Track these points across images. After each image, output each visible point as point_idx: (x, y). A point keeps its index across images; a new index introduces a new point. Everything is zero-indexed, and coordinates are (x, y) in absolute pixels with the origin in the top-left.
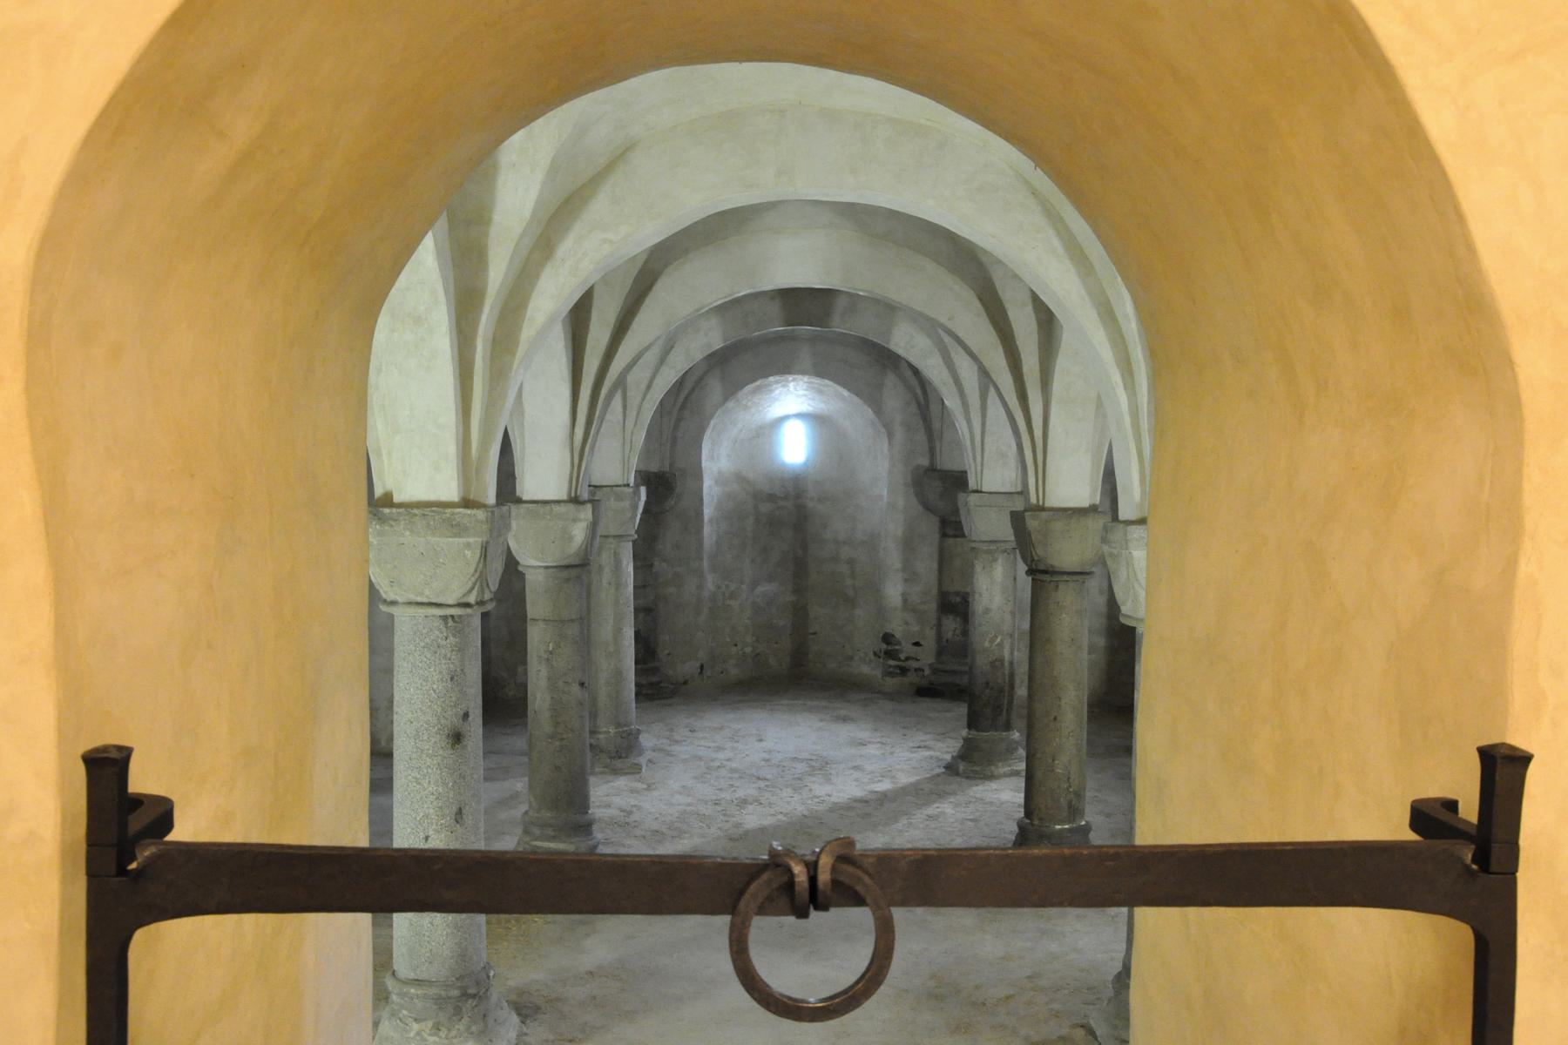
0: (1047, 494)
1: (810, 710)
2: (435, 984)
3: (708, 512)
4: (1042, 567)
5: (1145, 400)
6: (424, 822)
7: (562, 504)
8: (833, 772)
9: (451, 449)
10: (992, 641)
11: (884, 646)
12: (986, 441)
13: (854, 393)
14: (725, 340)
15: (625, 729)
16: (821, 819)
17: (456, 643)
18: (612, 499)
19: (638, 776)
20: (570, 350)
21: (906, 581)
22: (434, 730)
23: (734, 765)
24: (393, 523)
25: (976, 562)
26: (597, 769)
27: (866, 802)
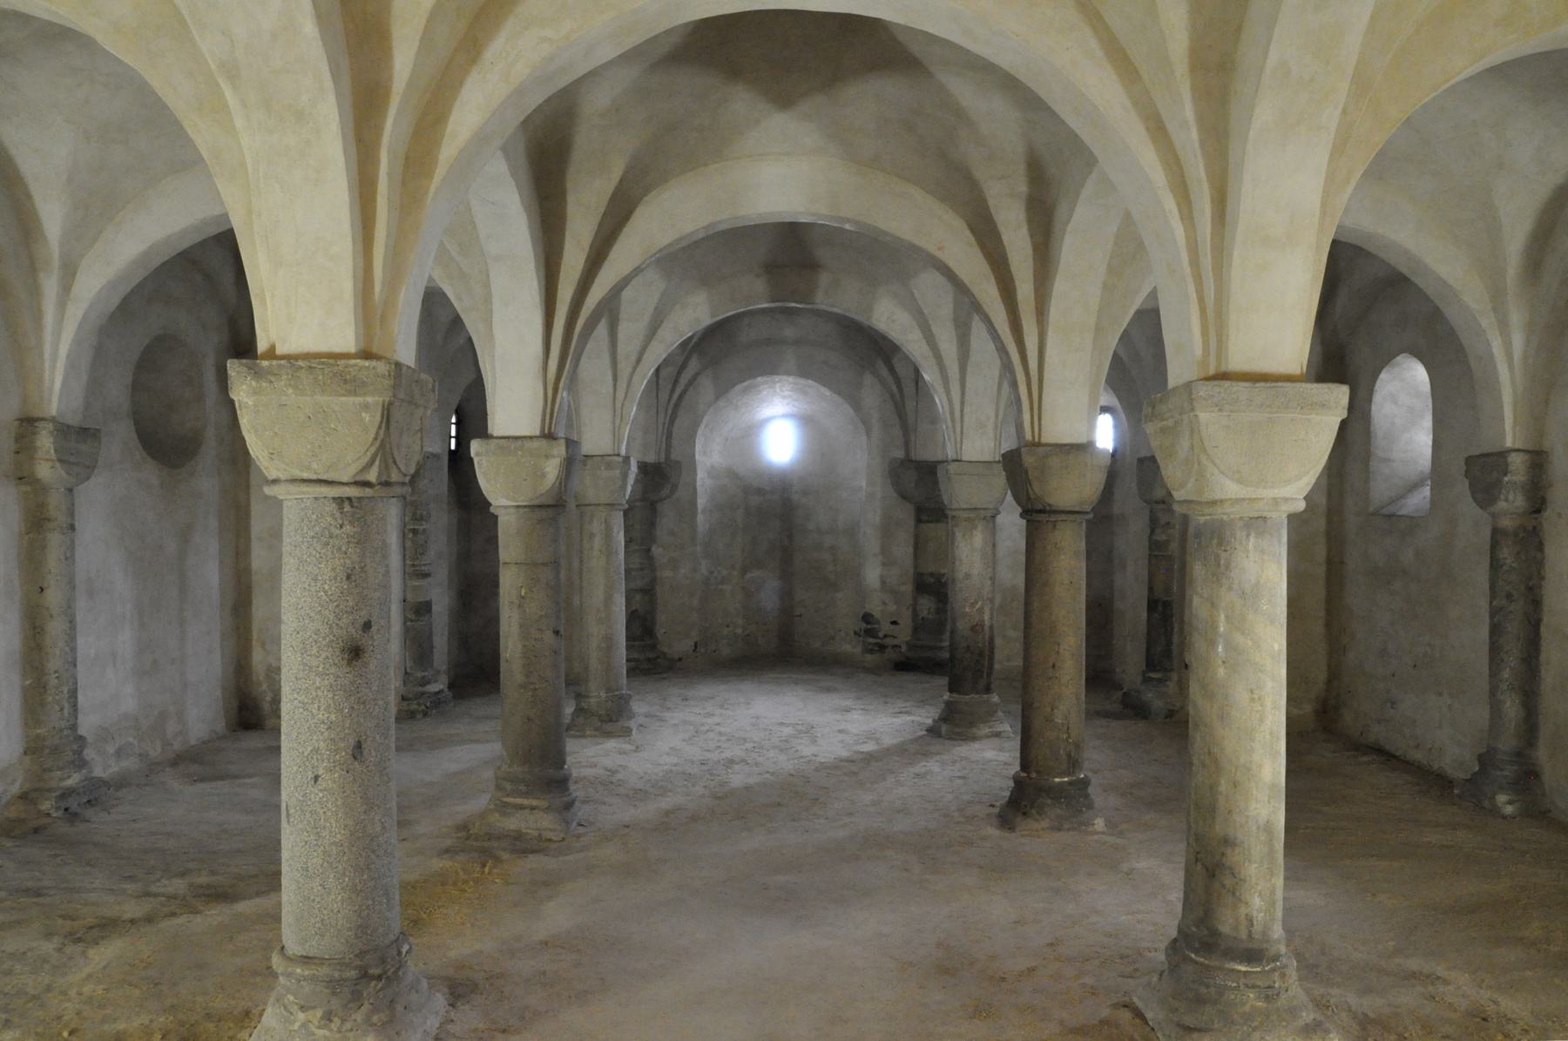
0: (1043, 430)
1: (796, 683)
2: (328, 962)
3: (701, 502)
4: (1040, 507)
5: (1208, 231)
6: (312, 758)
7: (535, 440)
8: (819, 735)
9: (347, 286)
10: (973, 605)
11: (864, 625)
12: (965, 410)
13: (835, 392)
14: (713, 316)
15: (616, 693)
16: (808, 778)
17: (355, 533)
18: (603, 468)
19: (627, 739)
20: (543, 290)
21: (884, 564)
22: (324, 642)
23: (722, 729)
24: (273, 379)
25: (956, 529)
26: (588, 733)
27: (853, 761)
